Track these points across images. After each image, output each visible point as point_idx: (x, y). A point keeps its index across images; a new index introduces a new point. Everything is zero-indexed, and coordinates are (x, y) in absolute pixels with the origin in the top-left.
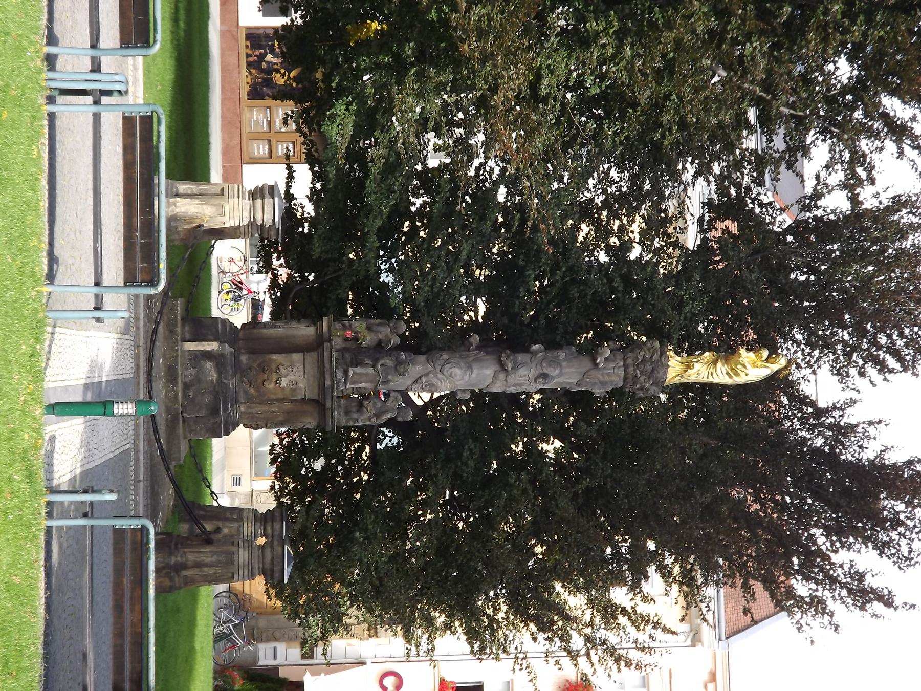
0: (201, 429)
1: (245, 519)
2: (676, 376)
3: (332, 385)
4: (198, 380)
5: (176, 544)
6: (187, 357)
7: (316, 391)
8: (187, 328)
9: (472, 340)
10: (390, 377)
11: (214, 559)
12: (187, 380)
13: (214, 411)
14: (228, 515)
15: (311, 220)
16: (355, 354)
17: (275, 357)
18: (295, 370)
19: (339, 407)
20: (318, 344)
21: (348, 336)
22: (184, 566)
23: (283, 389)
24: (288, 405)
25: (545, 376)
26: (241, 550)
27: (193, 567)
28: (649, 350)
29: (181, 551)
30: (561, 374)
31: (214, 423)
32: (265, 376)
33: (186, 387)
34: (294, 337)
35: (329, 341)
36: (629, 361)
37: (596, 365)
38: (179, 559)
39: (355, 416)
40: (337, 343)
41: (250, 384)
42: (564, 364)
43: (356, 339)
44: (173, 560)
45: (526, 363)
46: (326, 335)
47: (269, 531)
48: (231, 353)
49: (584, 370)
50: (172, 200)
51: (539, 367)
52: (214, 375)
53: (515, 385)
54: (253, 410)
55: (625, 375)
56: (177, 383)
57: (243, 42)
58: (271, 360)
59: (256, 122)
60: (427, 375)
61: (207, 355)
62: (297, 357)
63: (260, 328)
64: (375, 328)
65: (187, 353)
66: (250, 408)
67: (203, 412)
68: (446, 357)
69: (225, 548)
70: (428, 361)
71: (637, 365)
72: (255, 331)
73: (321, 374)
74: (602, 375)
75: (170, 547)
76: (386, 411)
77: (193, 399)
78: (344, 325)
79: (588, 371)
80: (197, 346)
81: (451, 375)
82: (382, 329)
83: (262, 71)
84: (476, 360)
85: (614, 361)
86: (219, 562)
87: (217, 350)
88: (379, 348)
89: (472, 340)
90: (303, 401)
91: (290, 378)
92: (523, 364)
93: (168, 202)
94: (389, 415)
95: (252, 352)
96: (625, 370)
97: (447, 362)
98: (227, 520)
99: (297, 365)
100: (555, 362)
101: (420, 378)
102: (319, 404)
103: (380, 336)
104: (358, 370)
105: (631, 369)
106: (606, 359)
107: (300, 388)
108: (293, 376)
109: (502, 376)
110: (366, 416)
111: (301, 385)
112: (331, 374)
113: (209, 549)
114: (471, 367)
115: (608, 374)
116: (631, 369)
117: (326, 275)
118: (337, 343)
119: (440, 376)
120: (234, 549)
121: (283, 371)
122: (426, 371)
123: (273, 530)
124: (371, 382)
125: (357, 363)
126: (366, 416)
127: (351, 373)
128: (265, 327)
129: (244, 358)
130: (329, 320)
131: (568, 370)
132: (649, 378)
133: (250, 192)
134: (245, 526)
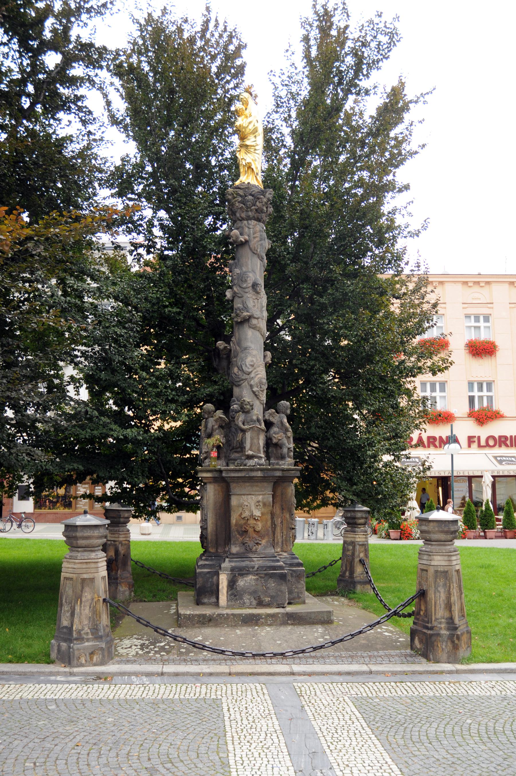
0: (297, 588)
1: (353, 540)
2: (257, 179)
3: (261, 470)
4: (254, 593)
5: (427, 628)
6: (233, 603)
7: (265, 484)
8: (206, 600)
9: (221, 347)
10: (255, 418)
11: (442, 590)
12: (254, 602)
13: (283, 577)
14: (349, 553)
15: (120, 484)
16: (231, 448)
17: (233, 521)
18: (246, 503)
19: (278, 464)
20: (225, 483)
21: (216, 454)
22: (451, 620)
23: (262, 514)
24: (277, 510)
25: (255, 286)
26: (433, 563)
27: (450, 611)
28: (234, 198)
29: (435, 624)
30: (253, 271)
31: (292, 575)
32: (251, 530)
33: (261, 604)
34: (215, 503)
35: (220, 471)
36: (243, 215)
37: (247, 242)
38: (443, 626)
39: (285, 450)
40: (220, 465)
41: (257, 544)
42: (244, 269)
43: (218, 447)
44: (444, 632)
45: (243, 302)
46: (216, 475)
47: (362, 521)
48: (230, 561)
49: (250, 253)
50: (75, 635)
51: (247, 290)
52: (250, 579)
53: (262, 311)
54: (280, 540)
55: (255, 220)
56: (259, 615)
57: (43, 511)
58: (236, 525)
59: (84, 505)
60: (251, 386)
61: (232, 584)
62: (234, 501)
63: (207, 534)
64: (209, 430)
65: (230, 603)
66: (278, 543)
67: (284, 588)
68: (236, 370)
69: (431, 579)
70: (239, 386)
71: (247, 208)
72: (209, 537)
73: (251, 479)
74: (254, 238)
75: (431, 635)
76: (282, 423)
77: (272, 597)
78: (205, 458)
79: (251, 249)
80: (223, 594)
81: (252, 366)
82: (210, 425)
83: (57, 502)
84: (239, 344)
85: (243, 228)
86: (445, 585)
87: (228, 574)
88: (228, 427)
89: (221, 347)
90: (274, 496)
91: (253, 508)
92: (243, 303)
93: (76, 639)
94: (285, 420)
95: (228, 541)
96: (251, 219)
97: (241, 369)
98: (353, 554)
99: (241, 501)
100: (242, 278)
101: (254, 392)
102: (278, 482)
103: (216, 427)
104: (248, 445)
105: (250, 213)
106: (241, 234)
107: (263, 499)
108: (251, 504)
109: (254, 322)
110: (285, 441)
111: (260, 498)
112: (252, 470)
113: (431, 595)
114: (246, 349)
115: (254, 233)
116: (250, 213)
117: (161, 472)
118: (220, 465)
119: (252, 375)
120: (431, 570)
121: (247, 514)
122: (248, 387)
123: (362, 518)
124: (258, 435)
125: (241, 447)
126: (285, 441)
127: (250, 453)
128: (206, 529)
129: (234, 549)
130: (202, 471)
131: (250, 267)
132: (258, 198)
133: (71, 550)
134: (358, 540)
